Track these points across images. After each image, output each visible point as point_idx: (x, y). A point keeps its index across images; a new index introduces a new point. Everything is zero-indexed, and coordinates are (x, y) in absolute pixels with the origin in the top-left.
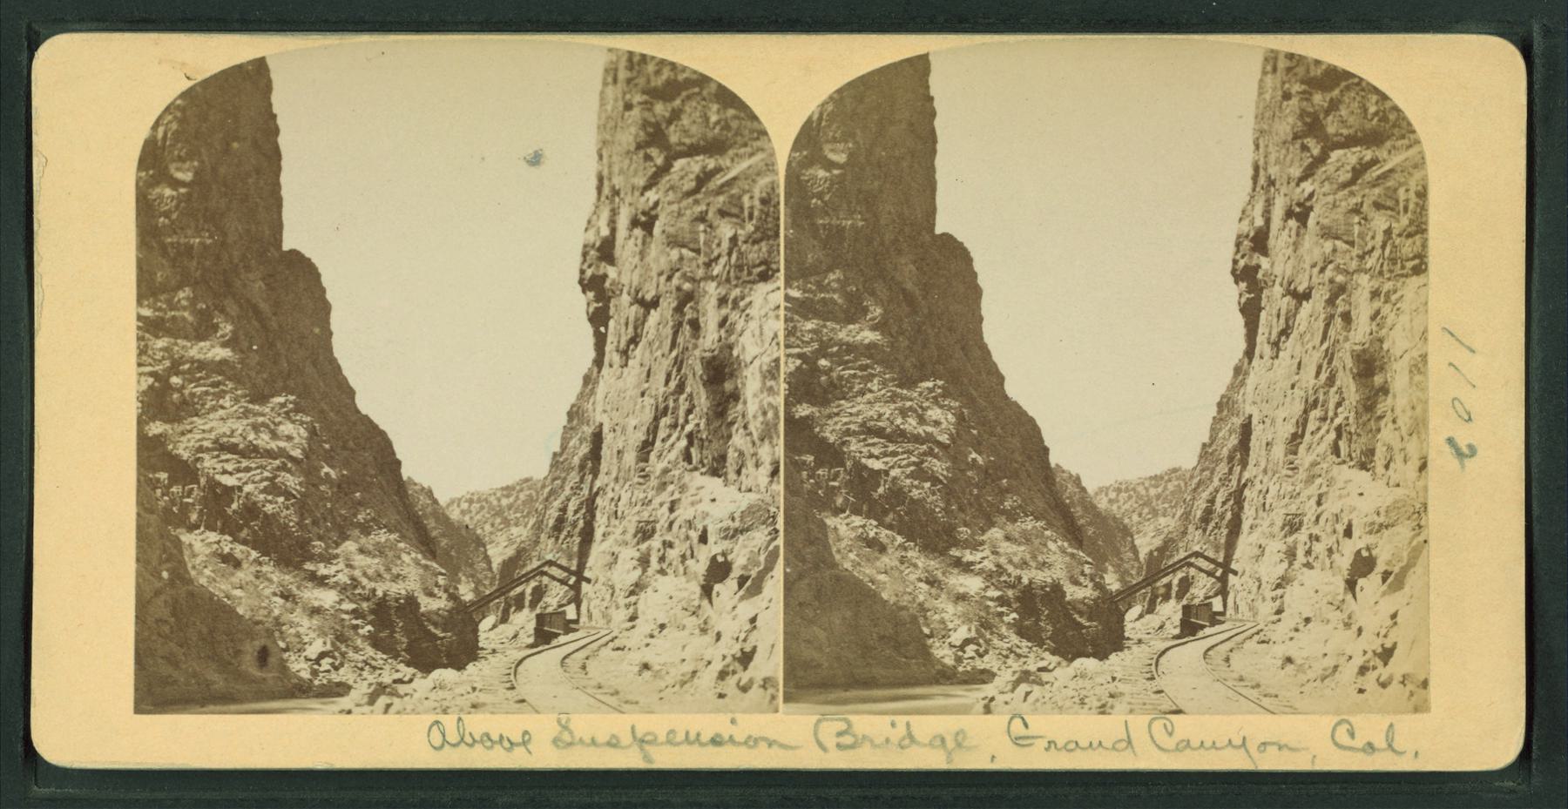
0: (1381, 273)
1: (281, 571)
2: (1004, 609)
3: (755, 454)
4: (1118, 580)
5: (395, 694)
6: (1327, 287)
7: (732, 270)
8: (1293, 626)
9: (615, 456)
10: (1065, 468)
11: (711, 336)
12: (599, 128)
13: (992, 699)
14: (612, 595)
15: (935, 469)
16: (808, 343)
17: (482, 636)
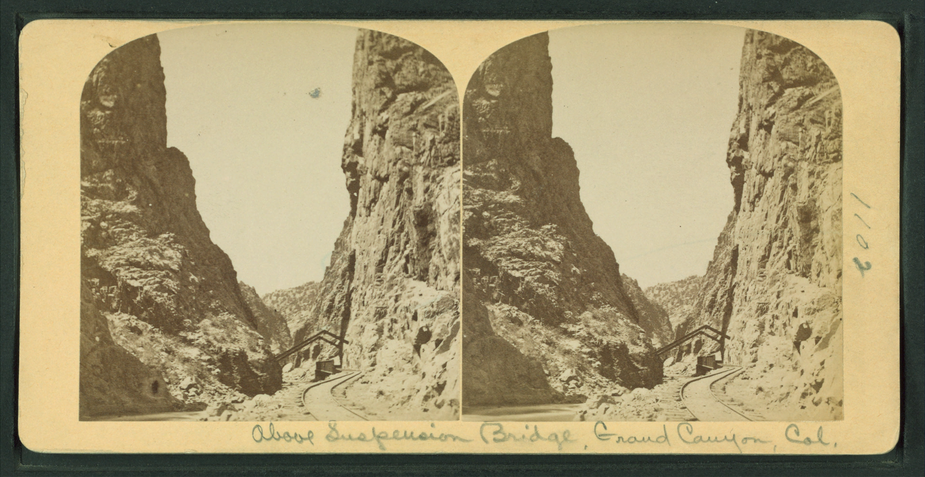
0: (815, 161)
1: (166, 337)
2: (592, 359)
3: (445, 268)
4: (660, 342)
5: (233, 409)
7: (432, 159)
11: (419, 198)
12: (353, 75)
13: (585, 412)
14: (361, 351)
15: (552, 276)
17: (284, 375)
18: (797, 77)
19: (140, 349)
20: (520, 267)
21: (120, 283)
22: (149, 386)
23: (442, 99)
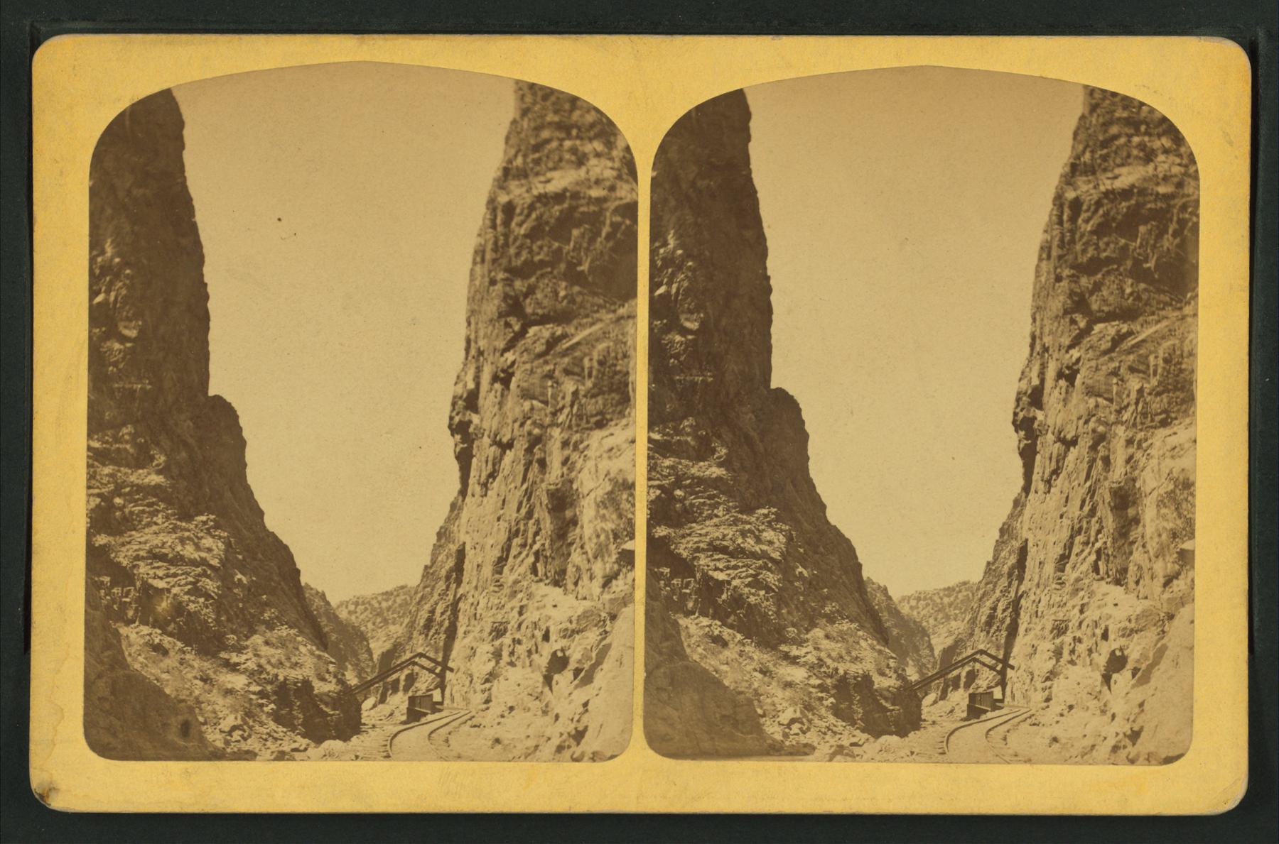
0: (1134, 425)
2: (264, 701)
3: (589, 570)
4: (356, 676)
6: (1090, 436)
7: (574, 419)
10: (312, 586)
11: (1119, 471)
12: (468, 299)
14: (1032, 680)
15: (769, 580)
16: (667, 477)
17: (364, 714)
18: (1111, 308)
20: (724, 567)
21: (138, 584)
23: (1156, 332)
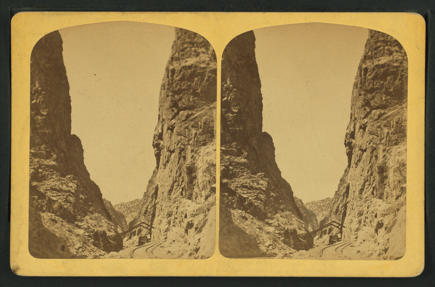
0: (386, 145)
1: (68, 224)
2: (90, 238)
4: (121, 230)
7: (387, 142)
8: (170, 242)
9: (162, 193)
10: (297, 197)
11: (380, 160)
12: (159, 102)
15: (261, 197)
16: (227, 162)
17: (124, 243)
18: (378, 105)
19: (56, 230)
21: (47, 199)
22: (60, 247)
23: (393, 113)
